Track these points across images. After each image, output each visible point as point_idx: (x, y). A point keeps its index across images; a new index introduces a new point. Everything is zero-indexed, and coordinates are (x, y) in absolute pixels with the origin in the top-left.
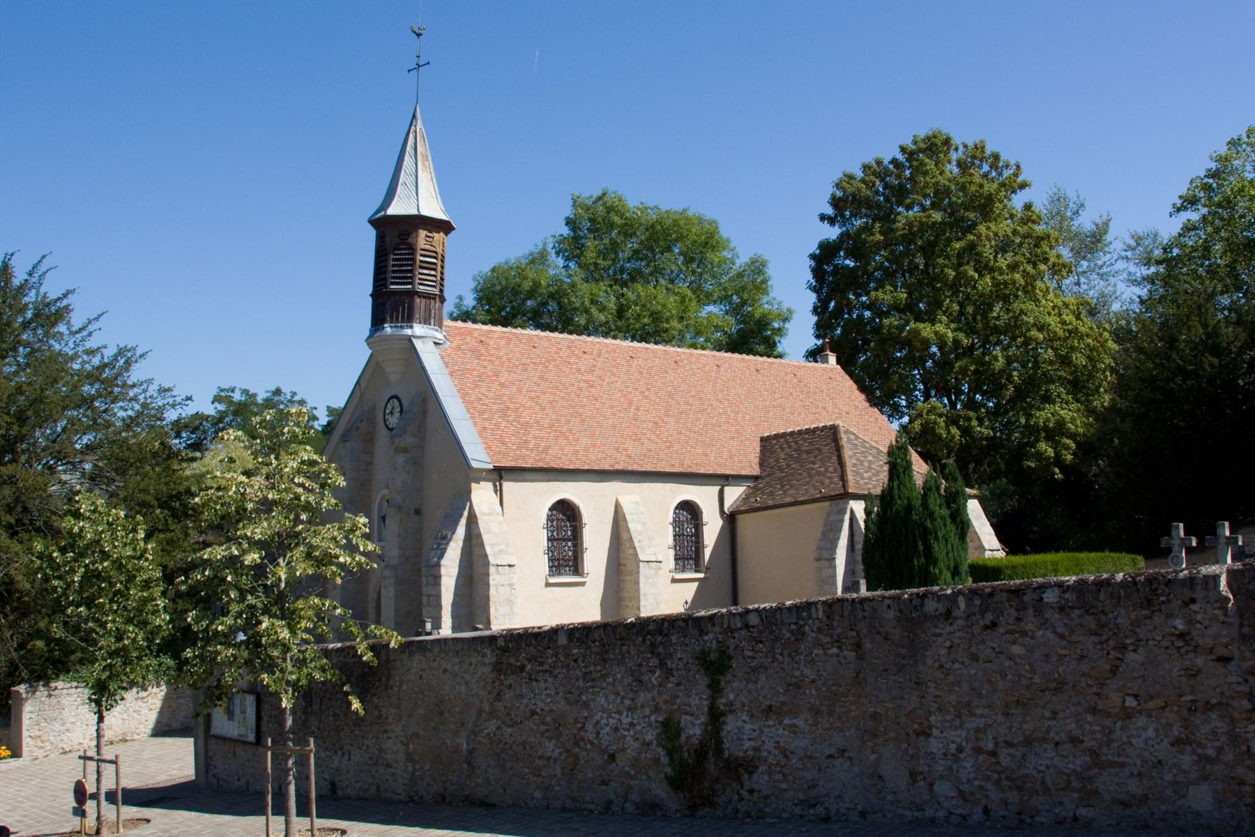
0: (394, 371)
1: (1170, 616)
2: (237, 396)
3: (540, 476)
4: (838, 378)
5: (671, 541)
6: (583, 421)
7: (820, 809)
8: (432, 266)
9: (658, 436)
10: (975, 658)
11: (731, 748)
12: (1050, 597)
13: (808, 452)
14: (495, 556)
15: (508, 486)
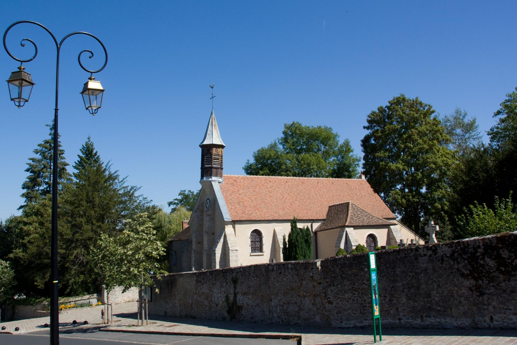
0: (208, 191)
1: (309, 272)
2: (187, 193)
3: (247, 222)
4: (364, 183)
6: (265, 204)
7: (254, 320)
8: (218, 159)
9: (291, 208)
10: (278, 281)
11: (239, 303)
12: (290, 266)
13: (340, 211)
15: (237, 226)
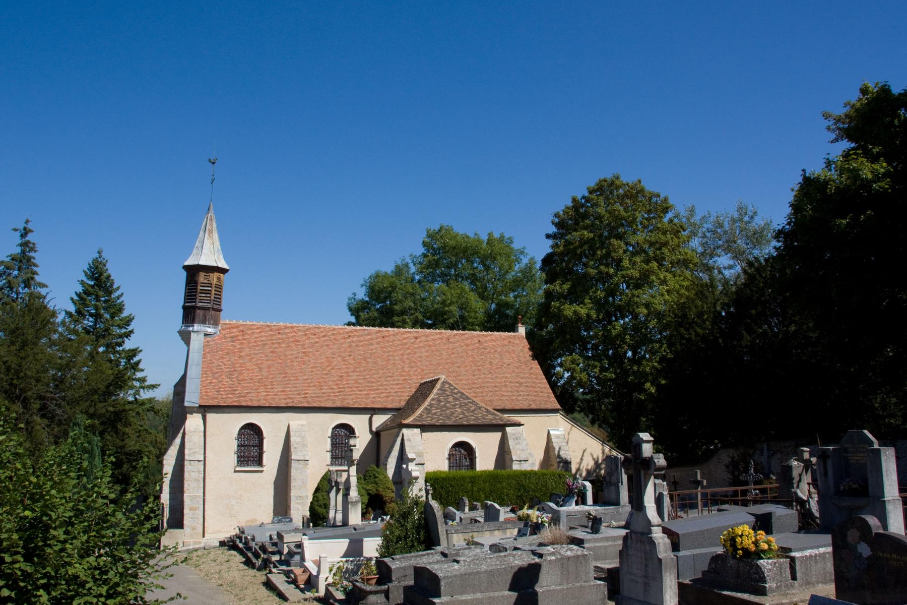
3: (242, 409)
5: (329, 447)
9: (337, 385)
14: (190, 455)
15: (210, 416)
